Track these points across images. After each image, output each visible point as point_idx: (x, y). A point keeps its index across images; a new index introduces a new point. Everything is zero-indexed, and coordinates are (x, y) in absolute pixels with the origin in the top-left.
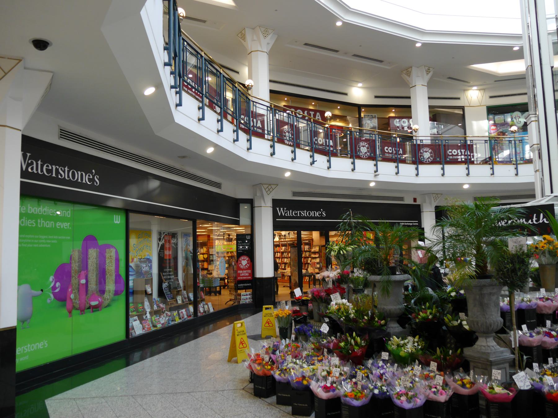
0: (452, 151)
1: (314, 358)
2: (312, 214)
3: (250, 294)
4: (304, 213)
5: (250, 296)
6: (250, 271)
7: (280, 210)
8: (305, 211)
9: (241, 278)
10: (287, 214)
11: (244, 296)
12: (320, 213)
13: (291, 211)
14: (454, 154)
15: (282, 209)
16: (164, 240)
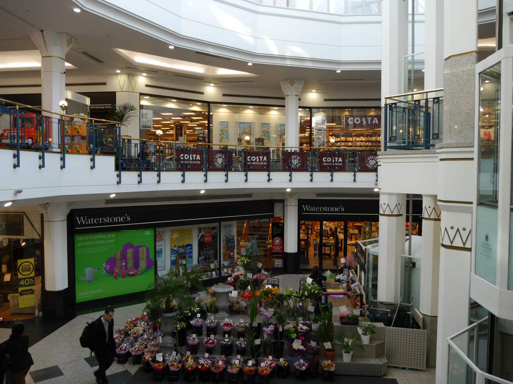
3: (281, 262)
4: (325, 209)
5: (281, 263)
6: (281, 247)
7: (305, 207)
8: (108, 218)
9: (275, 251)
12: (125, 218)
14: (186, 158)
15: (307, 206)
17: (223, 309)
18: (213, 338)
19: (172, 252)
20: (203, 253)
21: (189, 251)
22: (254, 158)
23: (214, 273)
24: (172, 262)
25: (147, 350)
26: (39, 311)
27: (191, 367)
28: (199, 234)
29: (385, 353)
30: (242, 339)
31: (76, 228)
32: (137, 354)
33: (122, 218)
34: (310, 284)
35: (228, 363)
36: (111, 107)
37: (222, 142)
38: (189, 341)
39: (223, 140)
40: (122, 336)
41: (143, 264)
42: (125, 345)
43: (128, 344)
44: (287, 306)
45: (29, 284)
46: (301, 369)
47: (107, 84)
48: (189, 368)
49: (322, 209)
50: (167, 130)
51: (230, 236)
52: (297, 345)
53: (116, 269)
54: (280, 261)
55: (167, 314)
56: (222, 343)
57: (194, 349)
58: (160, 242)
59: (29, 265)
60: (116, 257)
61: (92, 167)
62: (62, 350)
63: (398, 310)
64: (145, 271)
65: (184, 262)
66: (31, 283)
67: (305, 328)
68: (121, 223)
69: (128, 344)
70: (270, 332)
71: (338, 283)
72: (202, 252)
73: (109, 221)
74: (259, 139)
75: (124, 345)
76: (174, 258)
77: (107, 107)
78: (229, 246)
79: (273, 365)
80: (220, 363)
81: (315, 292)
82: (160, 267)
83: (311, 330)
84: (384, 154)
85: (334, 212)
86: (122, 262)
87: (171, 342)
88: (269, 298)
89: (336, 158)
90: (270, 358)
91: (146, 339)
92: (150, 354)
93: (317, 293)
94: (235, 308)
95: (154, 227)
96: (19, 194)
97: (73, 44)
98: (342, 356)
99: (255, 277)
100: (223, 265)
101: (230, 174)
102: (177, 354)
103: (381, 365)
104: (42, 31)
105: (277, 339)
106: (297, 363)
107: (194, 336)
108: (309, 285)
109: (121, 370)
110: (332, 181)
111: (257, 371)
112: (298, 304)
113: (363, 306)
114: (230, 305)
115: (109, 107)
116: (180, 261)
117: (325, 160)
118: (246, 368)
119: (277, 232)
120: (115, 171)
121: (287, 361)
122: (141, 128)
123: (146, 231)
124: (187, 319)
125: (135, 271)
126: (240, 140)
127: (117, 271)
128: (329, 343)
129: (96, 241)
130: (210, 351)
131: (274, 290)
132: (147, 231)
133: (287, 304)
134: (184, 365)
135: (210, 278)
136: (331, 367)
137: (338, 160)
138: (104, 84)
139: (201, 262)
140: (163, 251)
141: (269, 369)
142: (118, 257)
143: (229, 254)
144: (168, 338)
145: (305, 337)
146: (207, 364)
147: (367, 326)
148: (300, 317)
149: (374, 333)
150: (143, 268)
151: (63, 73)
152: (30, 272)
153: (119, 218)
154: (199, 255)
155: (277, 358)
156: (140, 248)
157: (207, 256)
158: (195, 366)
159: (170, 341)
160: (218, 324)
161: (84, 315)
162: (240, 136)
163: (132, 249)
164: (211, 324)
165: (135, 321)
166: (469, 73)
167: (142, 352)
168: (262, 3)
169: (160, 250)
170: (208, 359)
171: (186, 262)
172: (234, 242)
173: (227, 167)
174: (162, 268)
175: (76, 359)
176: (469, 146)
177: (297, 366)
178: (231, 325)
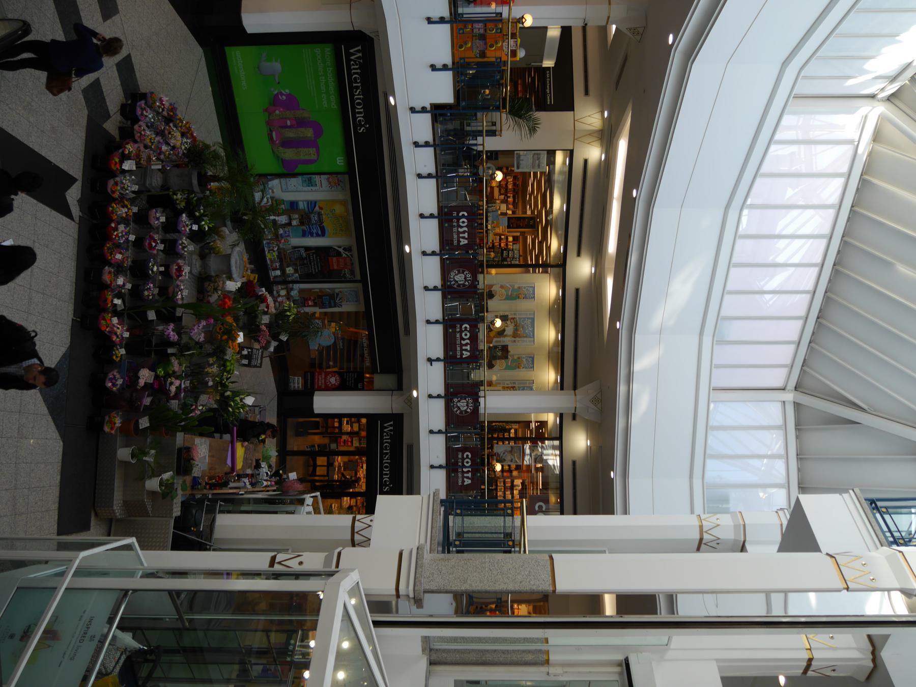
0: (467, 330)
1: (184, 292)
3: (298, 387)
6: (323, 387)
7: (391, 425)
8: (361, 97)
9: (317, 377)
10: (385, 436)
12: (363, 123)
13: (389, 441)
14: (463, 334)
15: (392, 428)
17: (204, 266)
18: (159, 248)
19: (311, 202)
23: (278, 273)
25: (142, 148)
27: (112, 211)
29: (132, 518)
30: (156, 291)
32: (135, 132)
33: (362, 119)
34: (244, 400)
35: (119, 269)
36: (549, 103)
38: (154, 210)
40: (165, 113)
41: (289, 154)
42: (150, 116)
43: (152, 120)
44: (208, 362)
46: (107, 381)
47: (587, 98)
48: (111, 209)
49: (387, 454)
50: (531, 207)
51: (340, 299)
53: (280, 111)
54: (300, 385)
56: (150, 262)
57: (141, 220)
63: (201, 542)
64: (278, 157)
65: (294, 223)
67: (173, 389)
69: (152, 120)
70: (166, 334)
71: (254, 464)
72: (313, 253)
74: (508, 352)
75: (150, 114)
76: (301, 206)
77: (548, 97)
78: (324, 297)
79: (114, 338)
80: (119, 256)
83: (169, 398)
85: (381, 474)
87: (154, 184)
88: (222, 337)
89: (470, 475)
90: (126, 335)
91: (160, 149)
92: (134, 152)
93: (229, 411)
94: (206, 284)
95: (350, 172)
98: (127, 446)
99: (263, 328)
100: (292, 289)
101: (438, 295)
102: (134, 192)
103: (112, 506)
105: (155, 346)
106: (118, 376)
107: (163, 219)
108: (241, 400)
109: (110, 108)
110: (432, 467)
111: (105, 310)
113: (208, 487)
114: (211, 276)
115: (549, 101)
116: (296, 216)
117: (467, 456)
121: (120, 360)
122: (516, 152)
123: (342, 158)
124: (190, 210)
127: (277, 112)
128: (148, 425)
130: (138, 243)
131: (234, 344)
132: (342, 161)
133: (210, 363)
134: (117, 202)
135: (270, 266)
137: (468, 478)
138: (587, 93)
140: (312, 188)
141: (107, 330)
143: (310, 299)
144: (159, 179)
145: (158, 389)
146: (117, 235)
147: (175, 487)
148: (190, 384)
149: (164, 498)
150: (282, 155)
153: (362, 115)
154: (307, 249)
155: (125, 345)
156: (314, 149)
157: (305, 261)
158: (114, 218)
159: (156, 181)
160: (181, 257)
162: (512, 318)
163: (313, 136)
164: (181, 245)
165: (192, 134)
166: (523, 583)
167: (139, 140)
168: (716, 344)
170: (126, 239)
172: (330, 307)
173: (448, 290)
174: (284, 187)
175: (129, 43)
177: (113, 374)
178: (178, 276)
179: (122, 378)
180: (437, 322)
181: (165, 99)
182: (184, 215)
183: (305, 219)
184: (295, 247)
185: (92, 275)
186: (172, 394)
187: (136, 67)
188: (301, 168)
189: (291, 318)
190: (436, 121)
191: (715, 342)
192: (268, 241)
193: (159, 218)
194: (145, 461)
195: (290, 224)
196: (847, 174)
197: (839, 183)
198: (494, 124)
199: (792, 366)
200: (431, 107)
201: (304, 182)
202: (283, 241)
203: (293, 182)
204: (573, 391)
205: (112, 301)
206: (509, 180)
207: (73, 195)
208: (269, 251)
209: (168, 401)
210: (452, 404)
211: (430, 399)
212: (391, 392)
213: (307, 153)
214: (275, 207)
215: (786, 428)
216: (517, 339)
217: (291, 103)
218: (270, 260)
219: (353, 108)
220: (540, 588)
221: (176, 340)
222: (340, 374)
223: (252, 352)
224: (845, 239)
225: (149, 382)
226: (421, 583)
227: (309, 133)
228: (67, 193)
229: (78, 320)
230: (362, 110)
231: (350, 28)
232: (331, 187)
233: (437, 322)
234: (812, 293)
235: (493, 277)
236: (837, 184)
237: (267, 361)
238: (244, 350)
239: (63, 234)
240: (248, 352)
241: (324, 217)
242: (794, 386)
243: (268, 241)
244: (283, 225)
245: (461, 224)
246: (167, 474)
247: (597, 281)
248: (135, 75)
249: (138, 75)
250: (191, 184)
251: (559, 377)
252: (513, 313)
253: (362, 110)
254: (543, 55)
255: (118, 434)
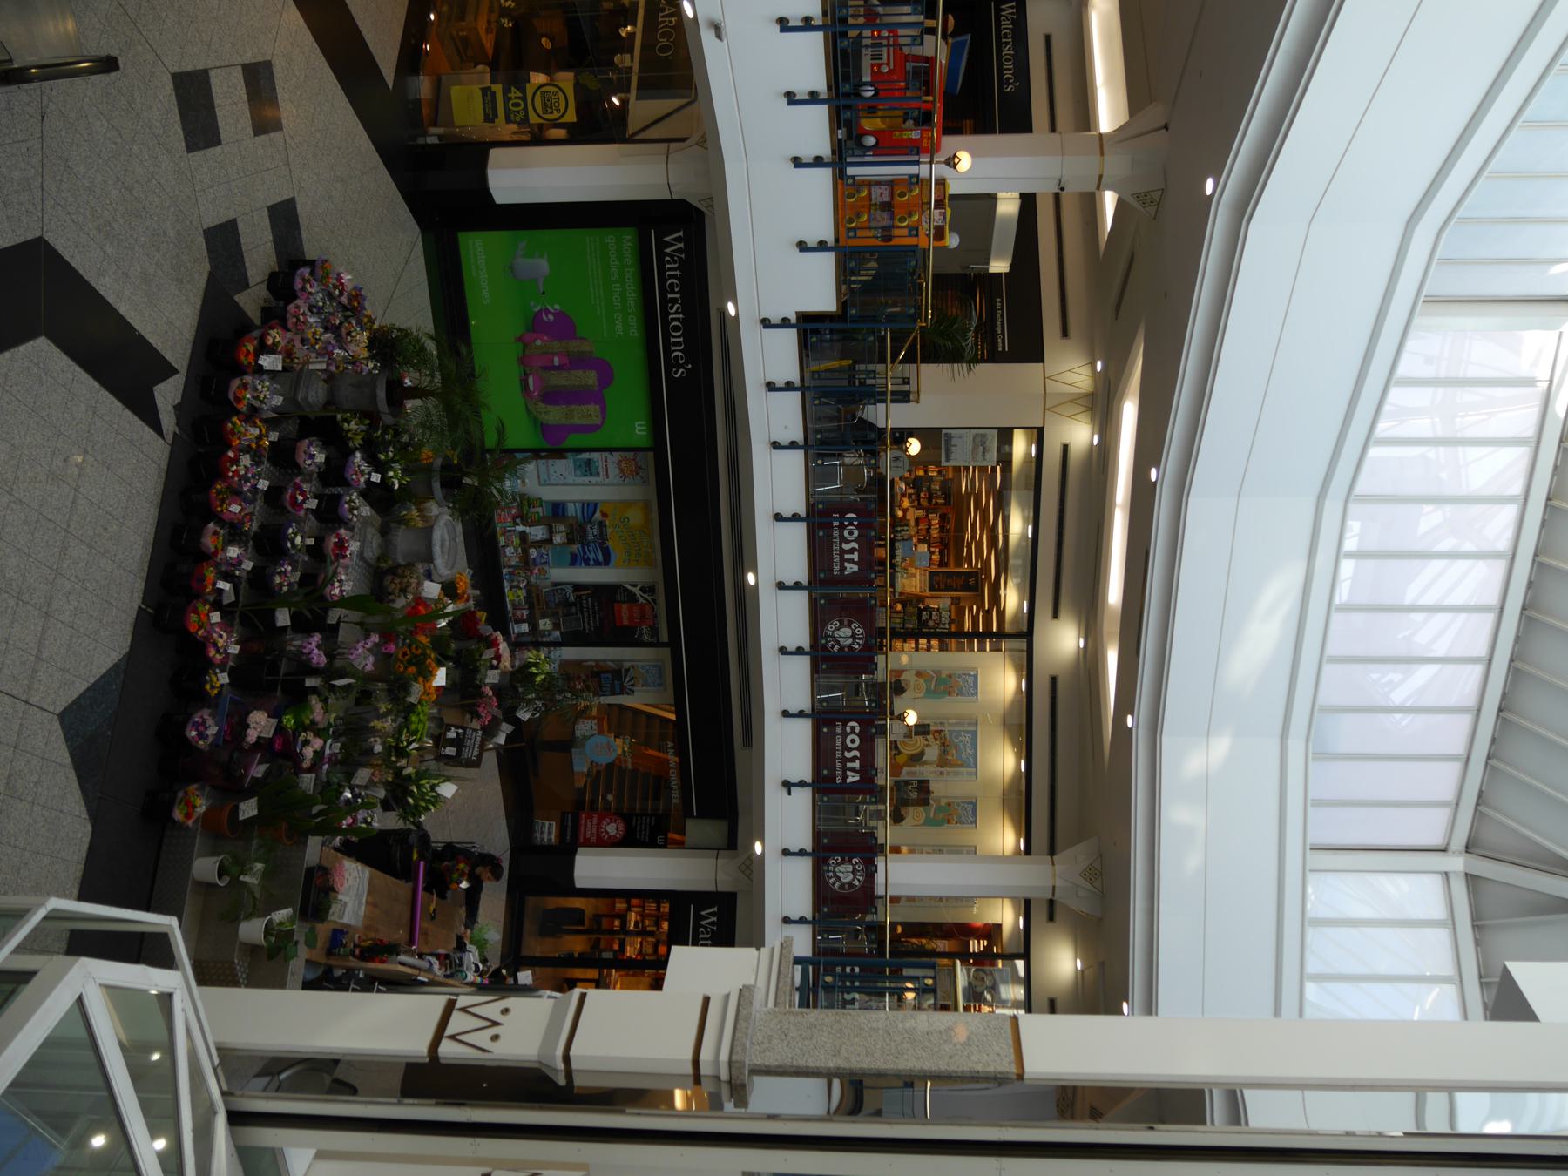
0: (855, 733)
1: (346, 582)
2: (677, 337)
3: (550, 840)
5: (546, 840)
6: (594, 840)
7: (712, 914)
8: (681, 316)
9: (583, 822)
10: (702, 933)
11: (549, 828)
12: (681, 362)
15: (715, 919)
16: (644, 602)
19: (588, 505)
20: (584, 597)
21: (591, 557)
22: (853, 741)
23: (525, 628)
24: (561, 506)
26: (440, 137)
28: (639, 586)
31: (653, 231)
32: (288, 316)
33: (680, 354)
35: (235, 533)
36: (1000, 349)
37: (916, 678)
38: (307, 441)
39: (922, 681)
40: (344, 299)
41: (554, 415)
45: (509, 110)
46: (189, 726)
47: (1065, 341)
51: (632, 679)
52: (260, 724)
53: (543, 340)
54: (553, 836)
55: (384, 386)
57: (282, 458)
58: (617, 471)
59: (558, 110)
60: (576, 338)
61: (804, 245)
62: (323, 154)
64: (535, 420)
65: (558, 539)
66: (512, 116)
67: (309, 752)
68: (668, 353)
72: (588, 596)
73: (673, 320)
74: (928, 792)
76: (572, 510)
77: (1000, 340)
78: (602, 675)
79: (212, 652)
80: (235, 508)
81: (412, 797)
82: (548, 470)
84: (784, 951)
86: (560, 355)
87: (310, 399)
88: (406, 668)
93: (409, 803)
96: (712, 33)
97: (1142, 209)
98: (213, 854)
104: (1166, 127)
105: (285, 675)
107: (320, 458)
108: (433, 788)
112: (378, 739)
113: (357, 952)
115: (1000, 345)
116: (562, 528)
118: (212, 572)
119: (638, 828)
120: (797, 313)
121: (220, 693)
122: (944, 431)
123: (643, 423)
125: (536, 394)
126: (921, 729)
127: (538, 342)
129: (618, 285)
130: (273, 496)
132: (644, 428)
133: (381, 711)
136: (185, 811)
138: (1065, 333)
139: (559, 591)
142: (573, 346)
144: (320, 391)
145: (281, 750)
151: (1062, 186)
152: (540, 111)
154: (577, 587)
156: (598, 407)
157: (573, 610)
158: (234, 444)
159: (315, 394)
161: (421, 244)
164: (346, 503)
168: (1313, 759)
169: (594, 471)
171: (559, 544)
172: (613, 693)
173: (822, 657)
174: (544, 477)
176: (736, 1043)
177: (202, 717)
179: (217, 725)
180: (801, 714)
181: (346, 277)
182: (358, 455)
183: (577, 533)
184: (556, 584)
185: (185, 536)
186: (306, 764)
187: (303, 222)
188: (573, 440)
189: (538, 679)
190: (806, 348)
191: (1310, 756)
192: (511, 570)
193: (314, 455)
194: (244, 883)
195: (549, 541)
196: (1535, 439)
197: (1510, 512)
198: (906, 381)
199: (1457, 804)
200: (798, 318)
201: (577, 467)
202: (536, 571)
203: (561, 467)
204: (1049, 857)
205: (214, 584)
206: (933, 522)
207: (168, 394)
208: (511, 588)
209: (296, 775)
210: (826, 868)
211: (785, 858)
212: (716, 851)
213: (587, 413)
214: (525, 508)
215: (1454, 924)
216: (946, 769)
217: (563, 327)
218: (513, 602)
219: (667, 336)
220: (992, 1069)
221: (322, 665)
222: (627, 818)
223: (464, 733)
224: (1541, 559)
225: (267, 736)
226: (744, 1050)
227: (590, 378)
228: (155, 388)
229: (150, 610)
230: (681, 339)
231: (712, 888)
232: (624, 477)
233: (801, 714)
234: (1497, 611)
235: (904, 657)
236: (1518, 457)
237: (490, 760)
238: (449, 730)
239: (141, 455)
240: (458, 734)
241: (609, 530)
242: (1464, 843)
243: (511, 570)
244: (538, 542)
245: (850, 745)
246: (282, 912)
247: (1090, 661)
248: (300, 234)
249: (304, 235)
250: (374, 397)
251: (1022, 840)
252: (938, 721)
253: (681, 339)
254: (990, 250)
255: (200, 829)
